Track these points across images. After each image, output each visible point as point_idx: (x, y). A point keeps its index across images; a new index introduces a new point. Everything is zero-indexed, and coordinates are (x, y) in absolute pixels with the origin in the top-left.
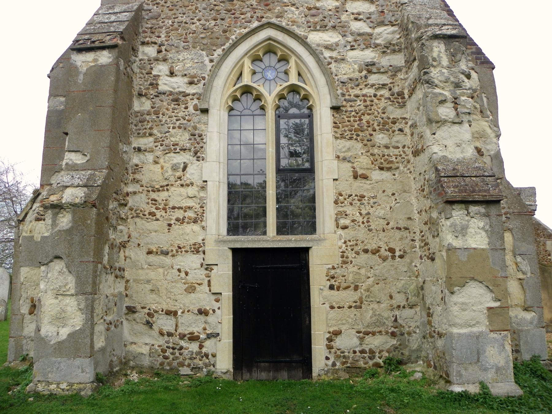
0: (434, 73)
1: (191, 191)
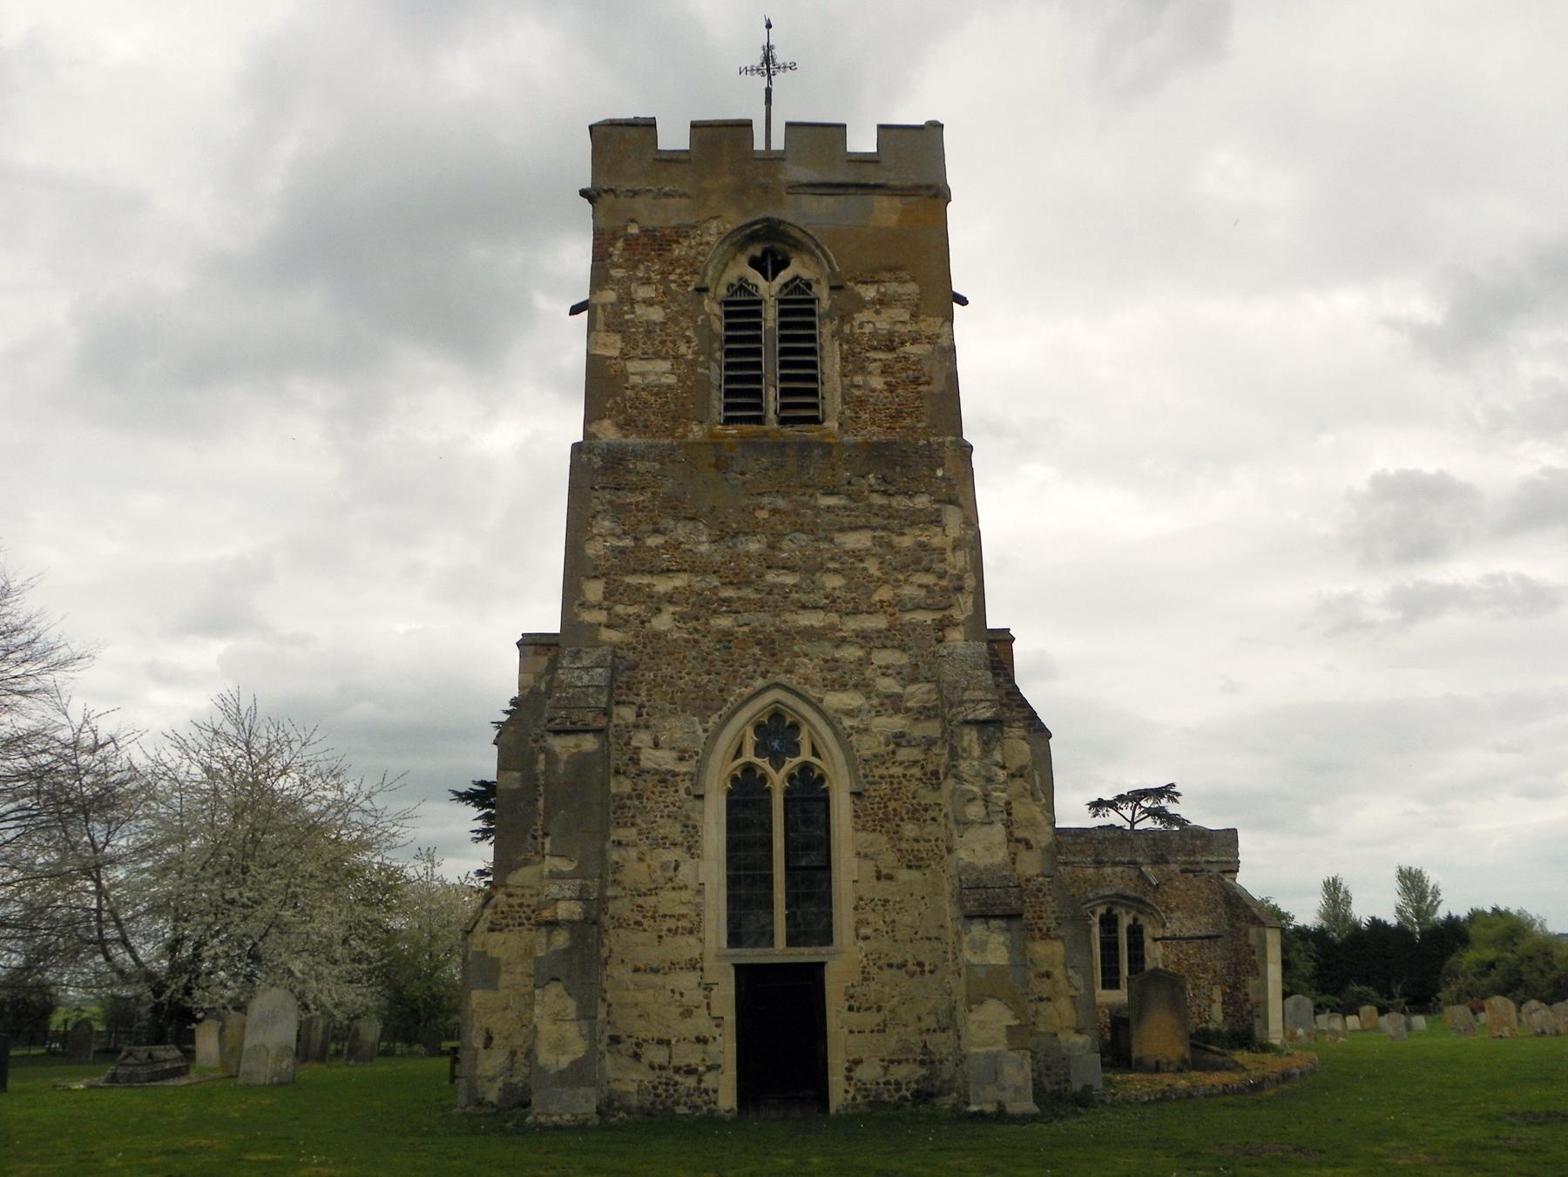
0: (964, 766)
1: (685, 896)
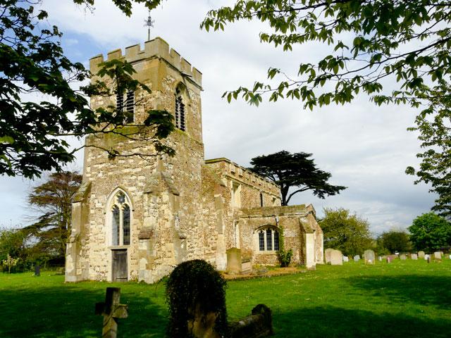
1: (103, 235)
